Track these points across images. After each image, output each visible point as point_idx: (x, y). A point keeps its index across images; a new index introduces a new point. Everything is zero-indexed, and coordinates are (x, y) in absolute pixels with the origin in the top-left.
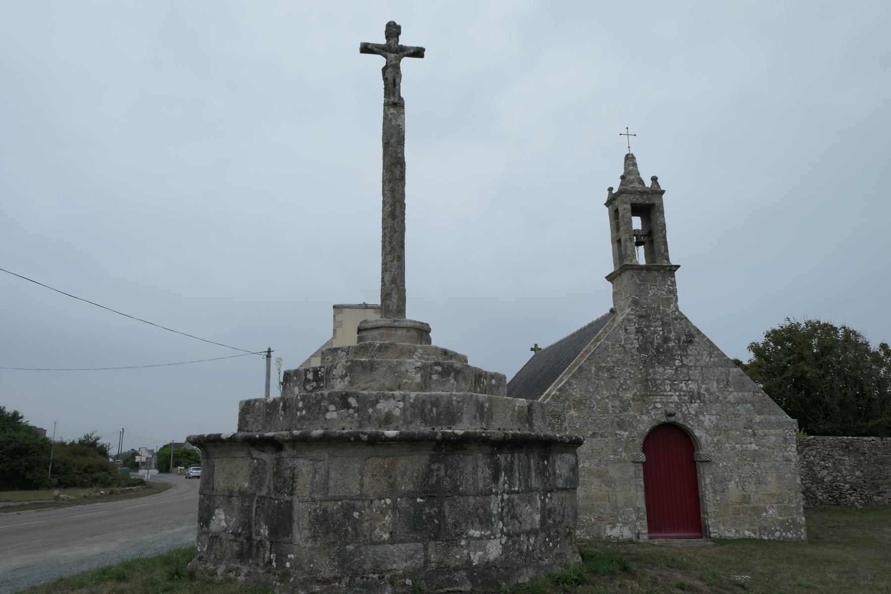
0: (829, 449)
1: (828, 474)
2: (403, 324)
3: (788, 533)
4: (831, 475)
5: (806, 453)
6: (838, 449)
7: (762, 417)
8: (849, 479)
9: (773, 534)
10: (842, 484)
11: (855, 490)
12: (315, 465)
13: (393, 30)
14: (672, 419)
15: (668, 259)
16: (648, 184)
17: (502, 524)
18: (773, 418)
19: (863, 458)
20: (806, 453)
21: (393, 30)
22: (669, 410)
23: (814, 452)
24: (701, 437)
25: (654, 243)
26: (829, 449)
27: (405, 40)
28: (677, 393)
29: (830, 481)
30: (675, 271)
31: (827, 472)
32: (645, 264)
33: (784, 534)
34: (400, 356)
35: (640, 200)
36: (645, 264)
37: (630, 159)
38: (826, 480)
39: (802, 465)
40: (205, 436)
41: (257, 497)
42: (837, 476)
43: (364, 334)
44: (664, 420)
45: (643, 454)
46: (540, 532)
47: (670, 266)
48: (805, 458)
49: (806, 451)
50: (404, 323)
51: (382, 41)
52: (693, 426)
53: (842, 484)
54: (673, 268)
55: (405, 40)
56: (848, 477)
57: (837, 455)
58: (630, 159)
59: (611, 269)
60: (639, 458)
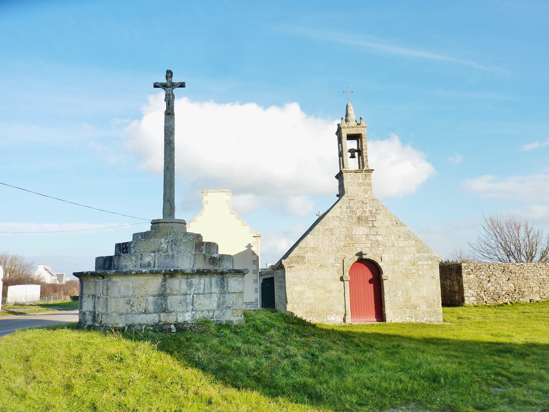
2: (174, 221)
3: (432, 318)
7: (420, 254)
9: (423, 319)
11: (508, 295)
13: (169, 74)
17: (58, 282)
18: (426, 255)
19: (514, 276)
21: (169, 74)
27: (176, 79)
28: (370, 242)
32: (95, 271)
33: (429, 319)
36: (95, 271)
40: (294, 108)
46: (216, 310)
50: (174, 220)
51: (164, 81)
52: (378, 260)
55: (176, 79)
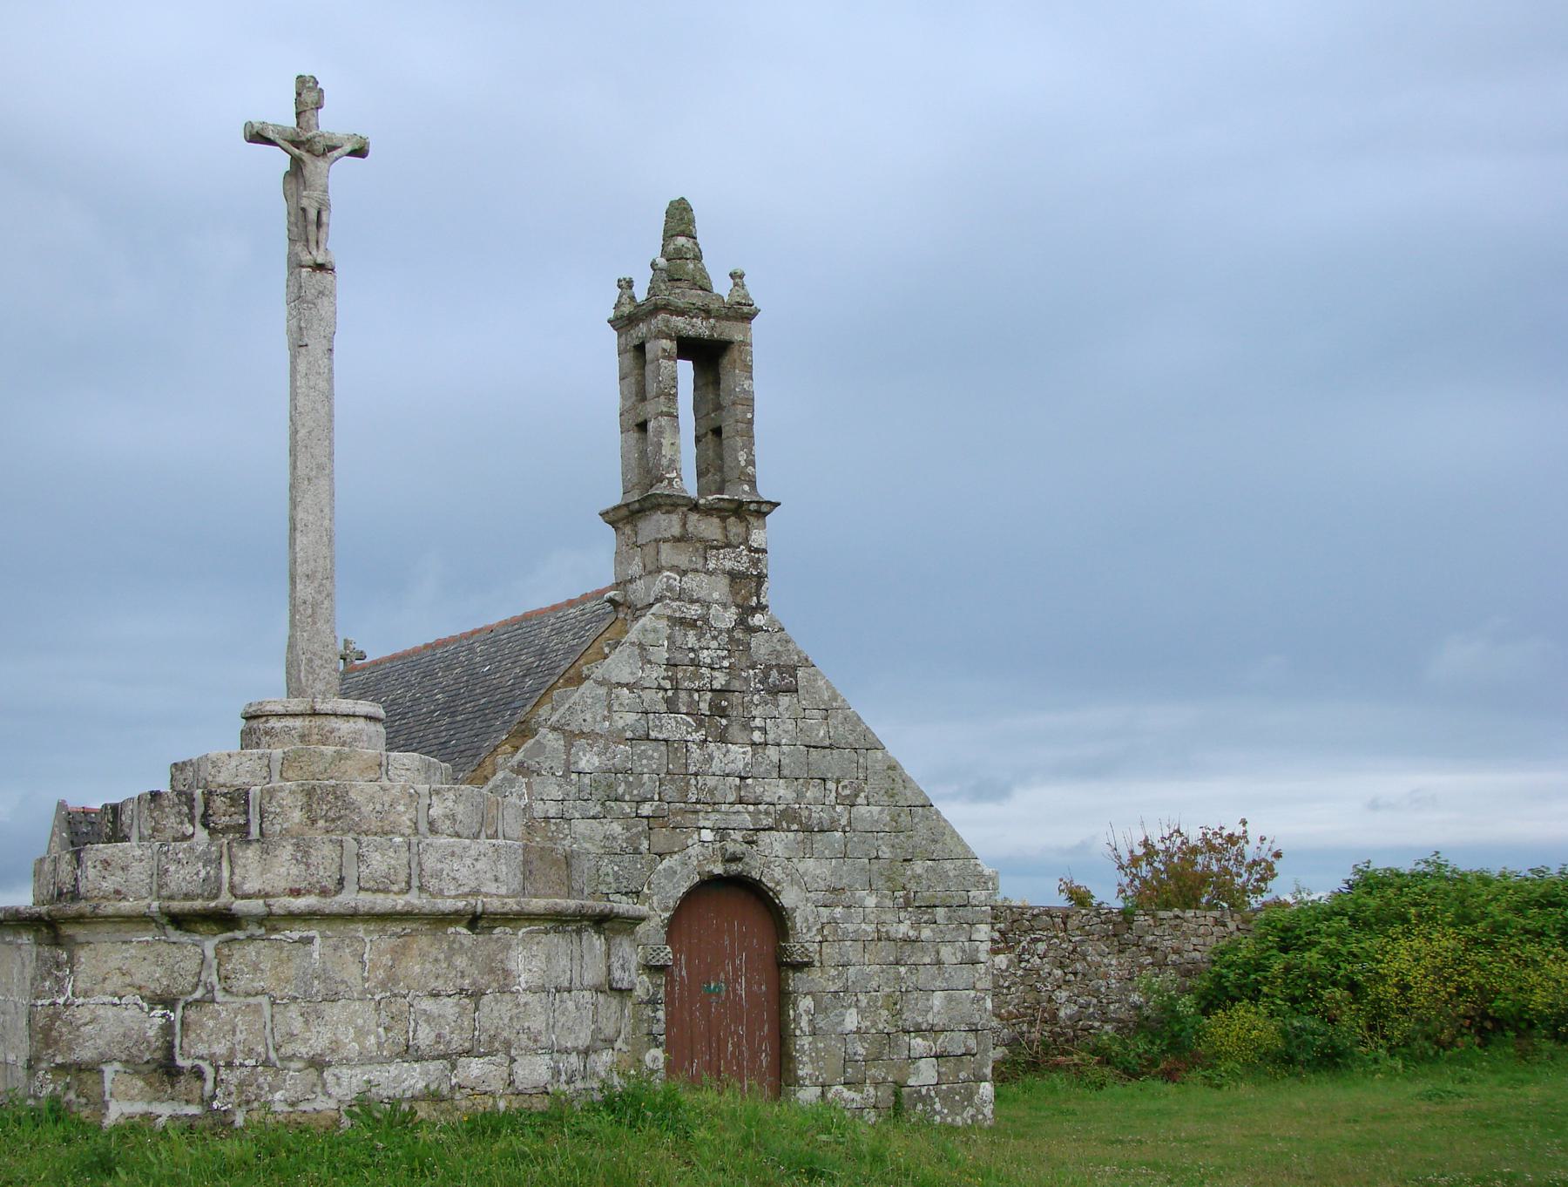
0: (1077, 938)
1: (1069, 1000)
4: (1075, 1002)
5: (1024, 947)
6: (1096, 937)
8: (1115, 1011)
10: (1097, 1024)
12: (1171, 1013)
14: (735, 868)
15: (752, 482)
16: (722, 287)
20: (1024, 947)
22: (731, 847)
23: (1041, 947)
24: (794, 910)
25: (724, 436)
26: (1077, 938)
29: (1070, 1018)
30: (766, 514)
31: (1067, 993)
34: (1320, 1064)
35: (700, 328)
37: (679, 218)
38: (1062, 1014)
39: (1012, 977)
41: (804, 1015)
42: (1088, 1005)
43: (254, 723)
44: (718, 869)
45: (669, 949)
47: (757, 502)
48: (1020, 962)
49: (1024, 943)
53: (1097, 1024)
54: (764, 508)
56: (1112, 1007)
57: (1094, 952)
58: (679, 218)
59: (614, 496)
60: (658, 958)
